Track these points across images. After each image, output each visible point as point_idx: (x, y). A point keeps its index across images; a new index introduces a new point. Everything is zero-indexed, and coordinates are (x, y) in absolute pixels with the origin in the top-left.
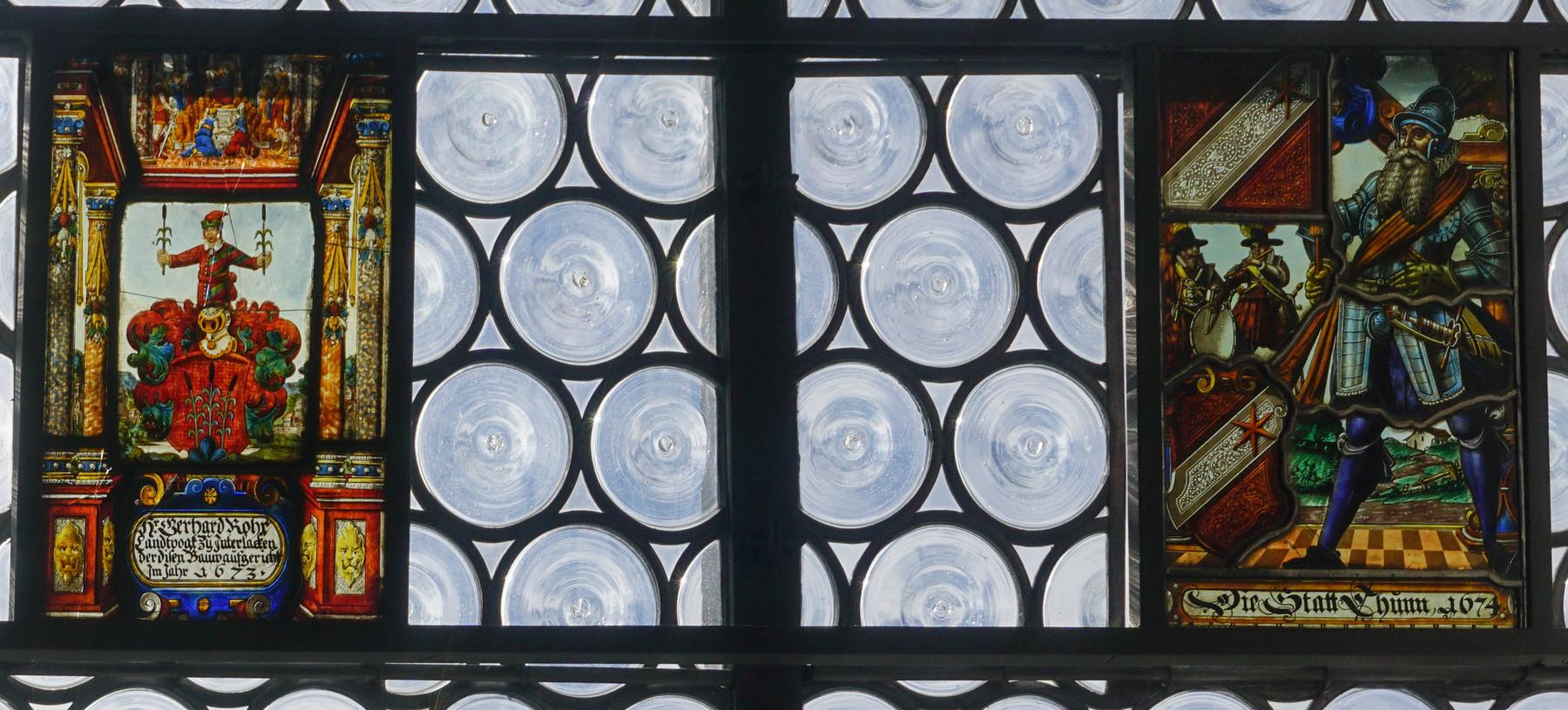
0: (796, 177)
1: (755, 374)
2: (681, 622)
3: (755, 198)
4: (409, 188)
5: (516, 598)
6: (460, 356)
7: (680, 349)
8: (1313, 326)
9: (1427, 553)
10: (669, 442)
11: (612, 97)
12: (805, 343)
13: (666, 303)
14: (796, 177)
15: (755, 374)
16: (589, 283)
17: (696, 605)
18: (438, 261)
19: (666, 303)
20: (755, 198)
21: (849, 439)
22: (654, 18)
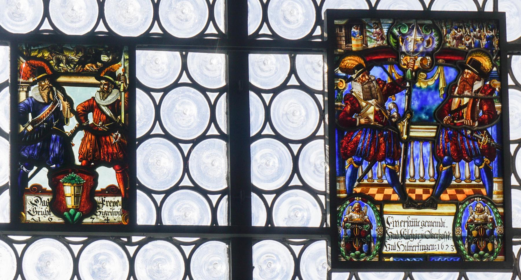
0: (73, 145)
1: (239, 143)
2: (219, 225)
3: (238, 87)
4: (134, 84)
5: (170, 215)
6: (148, 136)
7: (218, 134)
8: (425, 231)
9: (449, 195)
10: (213, 164)
11: (195, 59)
12: (253, 133)
13: (213, 119)
14: (73, 145)
15: (239, 143)
16: (187, 114)
17: (223, 221)
18: (143, 105)
19: (213, 119)
20: (238, 87)
21: (267, 164)
22: (250, 35)
